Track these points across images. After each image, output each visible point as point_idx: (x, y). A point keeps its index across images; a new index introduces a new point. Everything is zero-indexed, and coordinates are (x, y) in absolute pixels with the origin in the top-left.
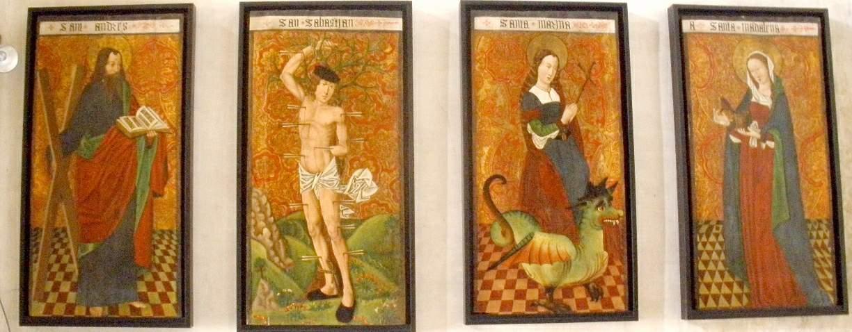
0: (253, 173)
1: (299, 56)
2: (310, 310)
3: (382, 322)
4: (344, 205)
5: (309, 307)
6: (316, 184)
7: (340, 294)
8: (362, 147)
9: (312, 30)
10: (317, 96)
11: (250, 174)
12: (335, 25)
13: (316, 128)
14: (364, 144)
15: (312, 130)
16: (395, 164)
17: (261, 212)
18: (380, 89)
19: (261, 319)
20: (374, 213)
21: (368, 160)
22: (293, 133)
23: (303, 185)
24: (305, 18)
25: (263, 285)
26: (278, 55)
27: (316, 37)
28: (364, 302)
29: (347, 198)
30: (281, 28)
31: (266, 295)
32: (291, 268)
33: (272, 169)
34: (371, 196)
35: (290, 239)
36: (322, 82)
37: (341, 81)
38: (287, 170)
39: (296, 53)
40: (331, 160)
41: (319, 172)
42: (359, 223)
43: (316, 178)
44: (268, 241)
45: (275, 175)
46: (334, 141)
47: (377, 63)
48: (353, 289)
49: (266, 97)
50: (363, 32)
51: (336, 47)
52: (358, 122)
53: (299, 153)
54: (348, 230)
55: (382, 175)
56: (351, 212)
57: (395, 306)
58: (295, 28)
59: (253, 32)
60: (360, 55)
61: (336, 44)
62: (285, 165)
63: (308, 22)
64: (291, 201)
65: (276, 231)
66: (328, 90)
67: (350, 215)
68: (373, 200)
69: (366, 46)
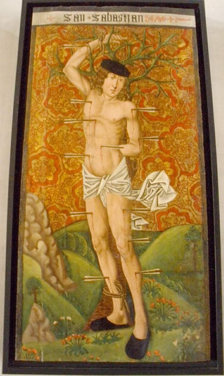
0: (27, 174)
1: (84, 50)
2: (94, 342)
3: (183, 358)
4: (139, 215)
5: (92, 339)
6: (103, 189)
7: (131, 323)
8: (157, 147)
9: (99, 25)
10: (104, 90)
11: (26, 176)
12: (123, 19)
13: (102, 124)
14: (159, 143)
15: (99, 127)
16: (194, 166)
17: (35, 221)
18: (175, 83)
19: (33, 353)
20: (173, 225)
21: (164, 161)
22: (76, 129)
23: (88, 190)
24: (92, 13)
25: (36, 311)
26: (62, 48)
27: (104, 31)
28: (160, 333)
29: (140, 205)
30: (66, 22)
31: (40, 322)
32: (72, 290)
33: (51, 171)
34: (168, 204)
35: (70, 255)
36: (111, 75)
37: (132, 74)
38: (68, 172)
39: (82, 46)
40: (120, 160)
41: (107, 175)
42: (156, 234)
43: (103, 182)
44: (43, 257)
45: (54, 179)
46: (124, 139)
47: (170, 57)
48: (147, 316)
49: (47, 91)
50: (153, 27)
51: (126, 41)
52: (151, 118)
53: (83, 151)
54: (141, 244)
55: (181, 179)
56: (144, 222)
57: (197, 337)
58: (80, 22)
59: (36, 26)
60: (152, 49)
61: (126, 38)
62: (66, 167)
63: (95, 17)
64: (72, 209)
65: (53, 245)
66: (117, 83)
67: (144, 226)
68: (172, 208)
69: (158, 41)
